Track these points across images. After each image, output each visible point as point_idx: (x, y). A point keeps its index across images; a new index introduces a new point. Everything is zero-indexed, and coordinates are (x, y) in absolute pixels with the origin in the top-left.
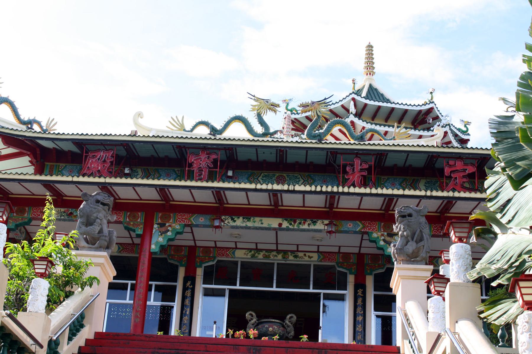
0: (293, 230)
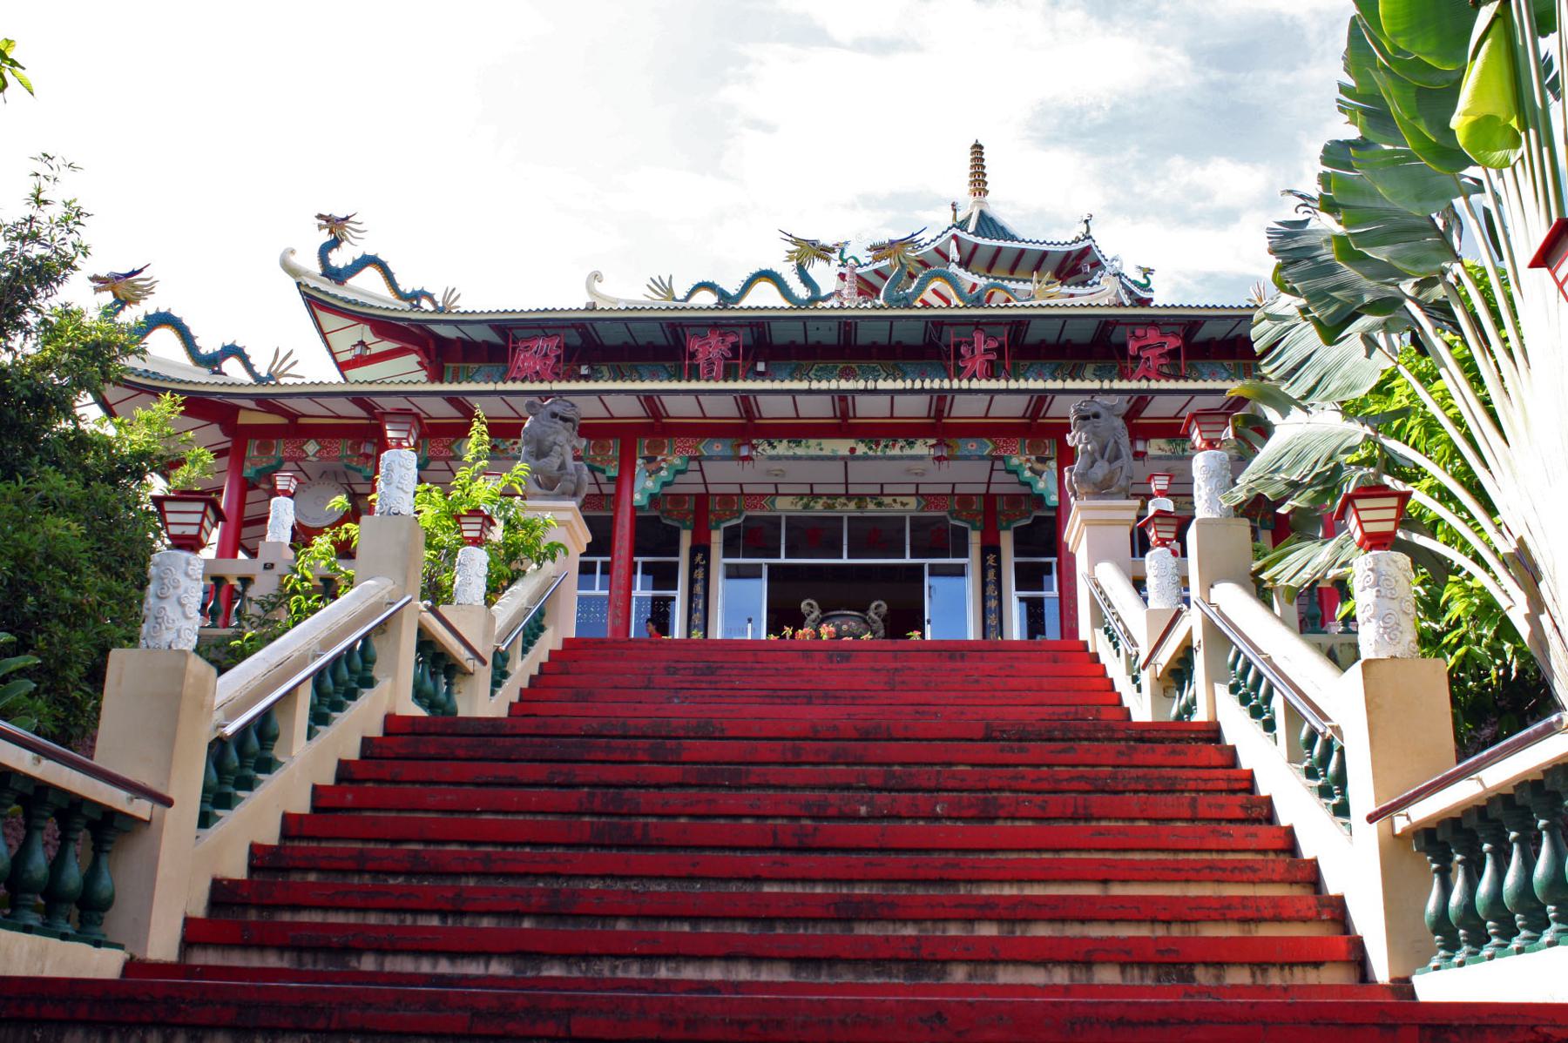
0: (876, 458)
